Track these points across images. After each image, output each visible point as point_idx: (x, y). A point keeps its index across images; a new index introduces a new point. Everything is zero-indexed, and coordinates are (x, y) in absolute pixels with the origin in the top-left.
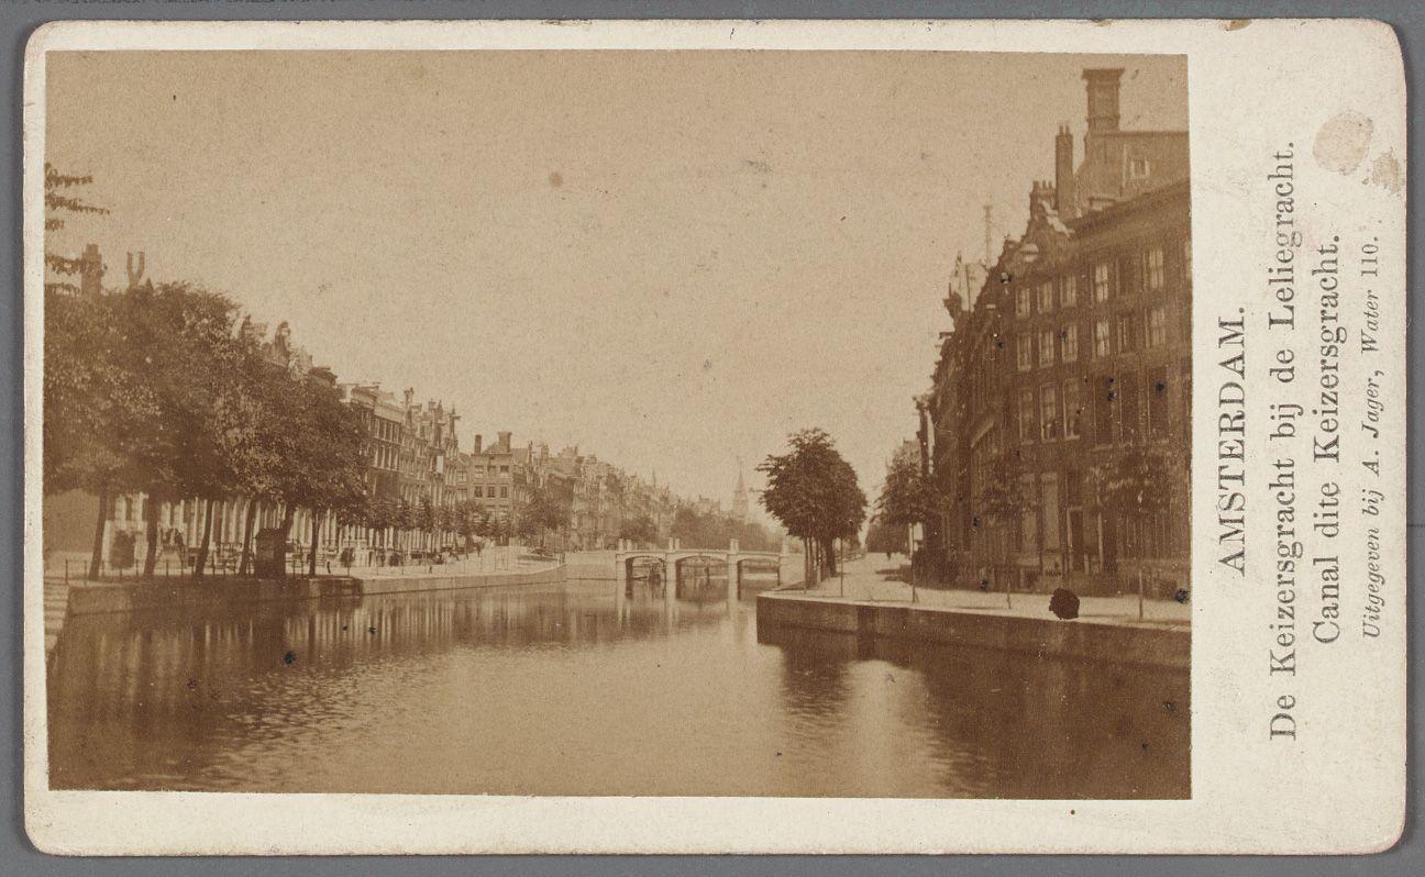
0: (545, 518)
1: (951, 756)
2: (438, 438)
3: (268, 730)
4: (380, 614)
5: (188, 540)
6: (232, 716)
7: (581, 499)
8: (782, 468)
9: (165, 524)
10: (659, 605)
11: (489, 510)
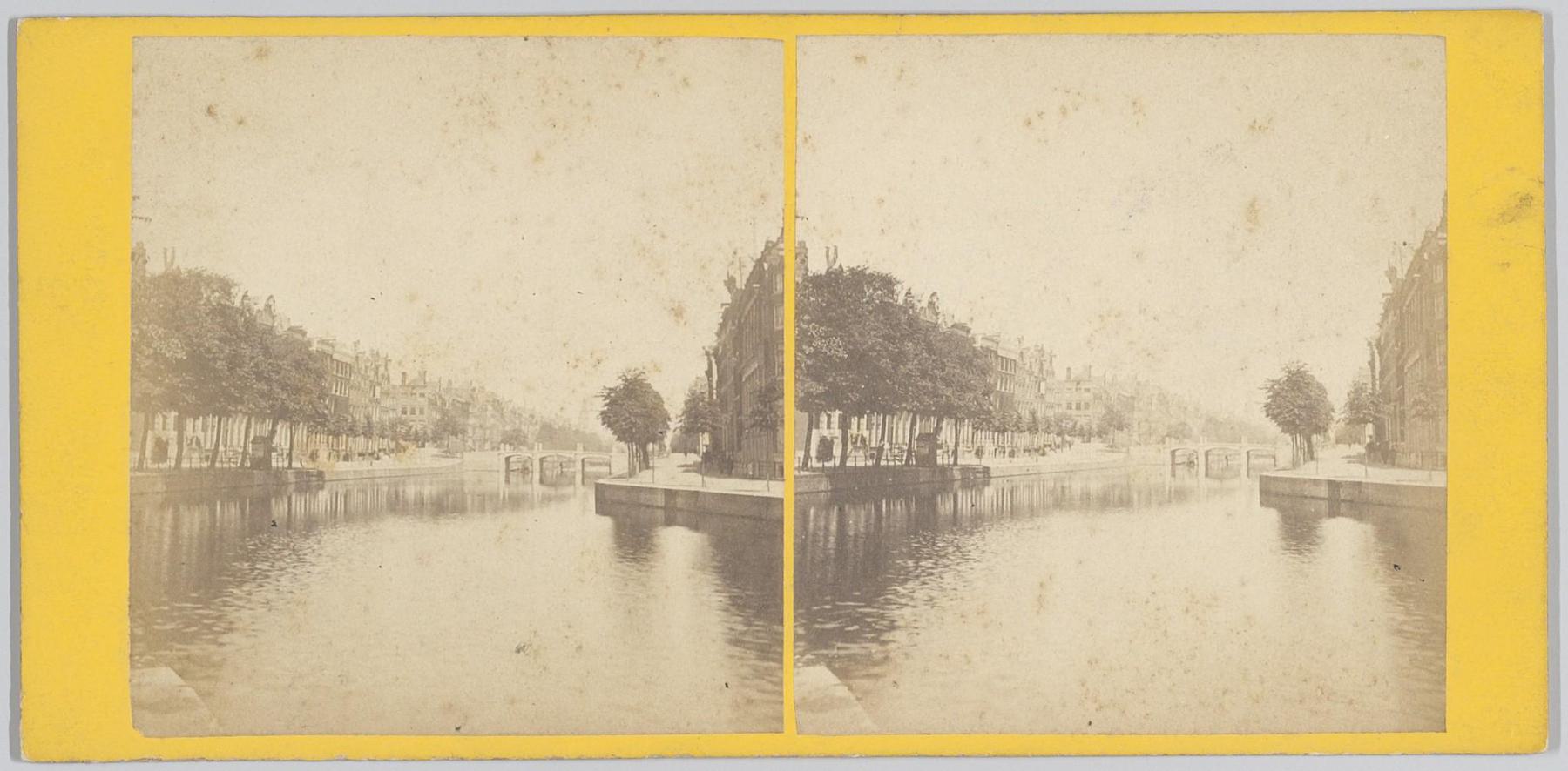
0: (1115, 423)
1: (728, 592)
2: (1041, 370)
3: (923, 571)
4: (1003, 490)
5: (870, 441)
6: (898, 562)
7: (475, 417)
8: (612, 395)
9: (189, 433)
10: (527, 488)
11: (411, 423)
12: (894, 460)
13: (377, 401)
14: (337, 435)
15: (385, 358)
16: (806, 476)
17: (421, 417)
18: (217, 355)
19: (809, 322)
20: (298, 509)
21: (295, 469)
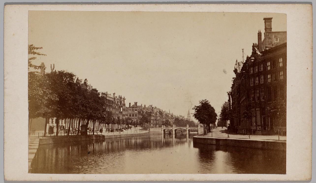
3: (84, 169)
5: (66, 127)
8: (198, 108)
12: (74, 133)
13: (122, 112)
14: (108, 124)
15: (123, 99)
16: (45, 139)
17: (136, 117)
18: (69, 99)
19: (46, 89)
20: (96, 148)
21: (95, 135)
